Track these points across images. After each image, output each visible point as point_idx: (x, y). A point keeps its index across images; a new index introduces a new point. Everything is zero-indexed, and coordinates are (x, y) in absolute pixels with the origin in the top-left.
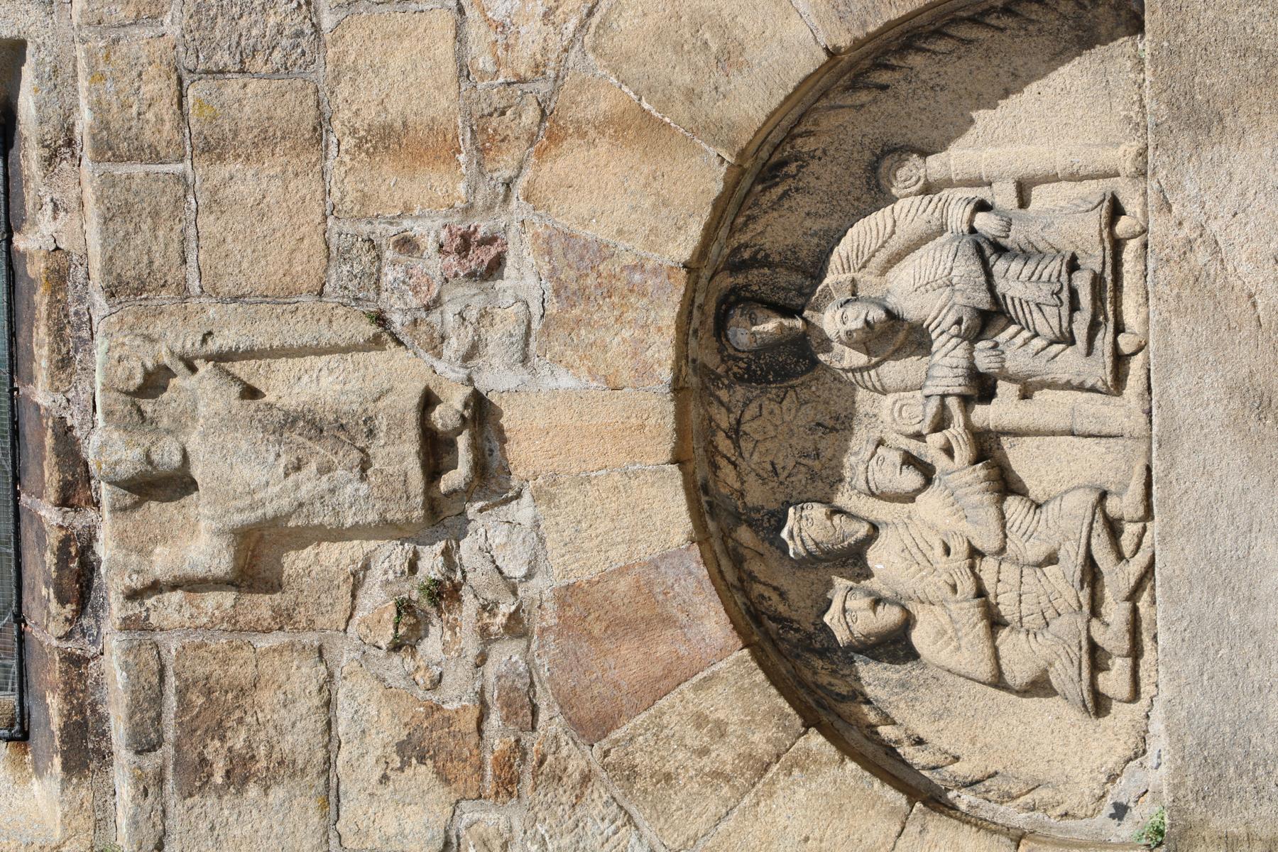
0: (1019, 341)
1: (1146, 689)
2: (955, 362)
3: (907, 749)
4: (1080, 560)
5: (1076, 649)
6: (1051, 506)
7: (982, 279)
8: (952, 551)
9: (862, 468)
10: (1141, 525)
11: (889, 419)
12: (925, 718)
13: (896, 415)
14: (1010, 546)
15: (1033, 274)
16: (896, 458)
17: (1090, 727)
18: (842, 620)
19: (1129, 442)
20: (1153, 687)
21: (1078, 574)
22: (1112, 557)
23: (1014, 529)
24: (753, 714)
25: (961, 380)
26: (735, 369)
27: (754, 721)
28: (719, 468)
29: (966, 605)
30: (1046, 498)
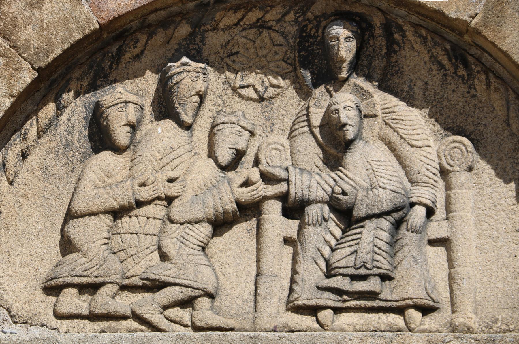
0: (329, 237)
1: (65, 324)
2: (313, 190)
3: (19, 146)
4: (163, 278)
5: (95, 274)
6: (204, 258)
7: (376, 211)
8: (171, 184)
9: (234, 119)
10: (189, 323)
11: (270, 141)
12: (42, 161)
13: (273, 146)
14: (174, 227)
15: (379, 248)
16: (241, 145)
17: (35, 283)
18: (119, 101)
19: (251, 316)
20: (66, 330)
21: (152, 276)
22: (165, 302)
23: (187, 230)
24: (48, 29)
25: (299, 194)
26: (310, 26)
27: (43, 29)
28: (235, 12)
29: (130, 193)
30: (209, 254)
